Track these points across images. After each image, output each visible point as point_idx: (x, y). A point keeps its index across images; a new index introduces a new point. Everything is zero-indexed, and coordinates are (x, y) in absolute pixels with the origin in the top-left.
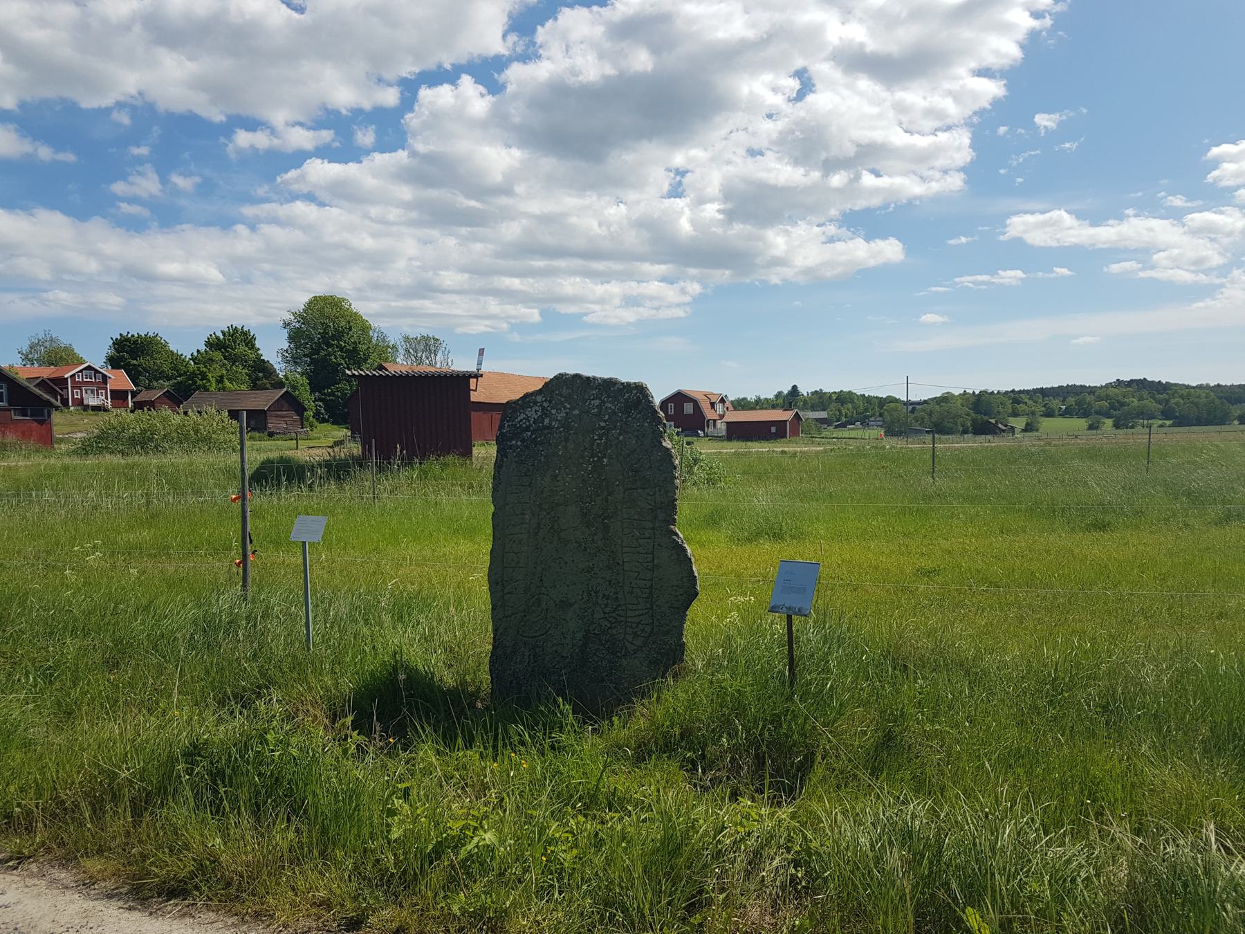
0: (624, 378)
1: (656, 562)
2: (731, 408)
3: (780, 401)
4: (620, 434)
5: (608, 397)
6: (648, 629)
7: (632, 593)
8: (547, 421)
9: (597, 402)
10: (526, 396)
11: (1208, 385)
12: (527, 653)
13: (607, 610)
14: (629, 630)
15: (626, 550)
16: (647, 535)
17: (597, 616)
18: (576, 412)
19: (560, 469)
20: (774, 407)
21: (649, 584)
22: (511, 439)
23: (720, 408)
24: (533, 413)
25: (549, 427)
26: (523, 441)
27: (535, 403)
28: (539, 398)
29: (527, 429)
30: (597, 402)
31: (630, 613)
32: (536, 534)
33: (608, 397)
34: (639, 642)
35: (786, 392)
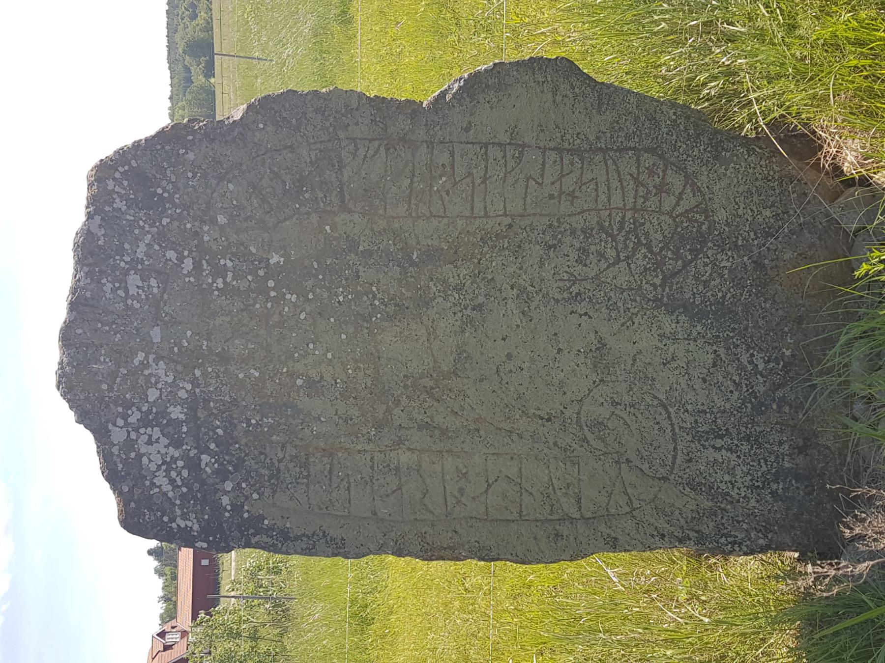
0: (74, 213)
1: (504, 138)
2: (173, 623)
3: (167, 570)
4: (213, 221)
5: (121, 252)
6: (648, 160)
7: (572, 195)
8: (177, 413)
9: (134, 280)
10: (111, 474)
11: (170, 109)
12: (711, 454)
13: (611, 253)
14: (653, 203)
15: (479, 205)
16: (445, 158)
17: (623, 280)
18: (156, 334)
19: (292, 375)
20: (175, 577)
21: (553, 155)
22: (218, 508)
23: (170, 638)
24: (155, 451)
25: (192, 405)
26: (222, 474)
27: (129, 444)
28: (118, 435)
29: (193, 465)
30: (134, 280)
31: (616, 200)
32: (444, 432)
33: (121, 252)
34: (676, 182)
35: (156, 563)
